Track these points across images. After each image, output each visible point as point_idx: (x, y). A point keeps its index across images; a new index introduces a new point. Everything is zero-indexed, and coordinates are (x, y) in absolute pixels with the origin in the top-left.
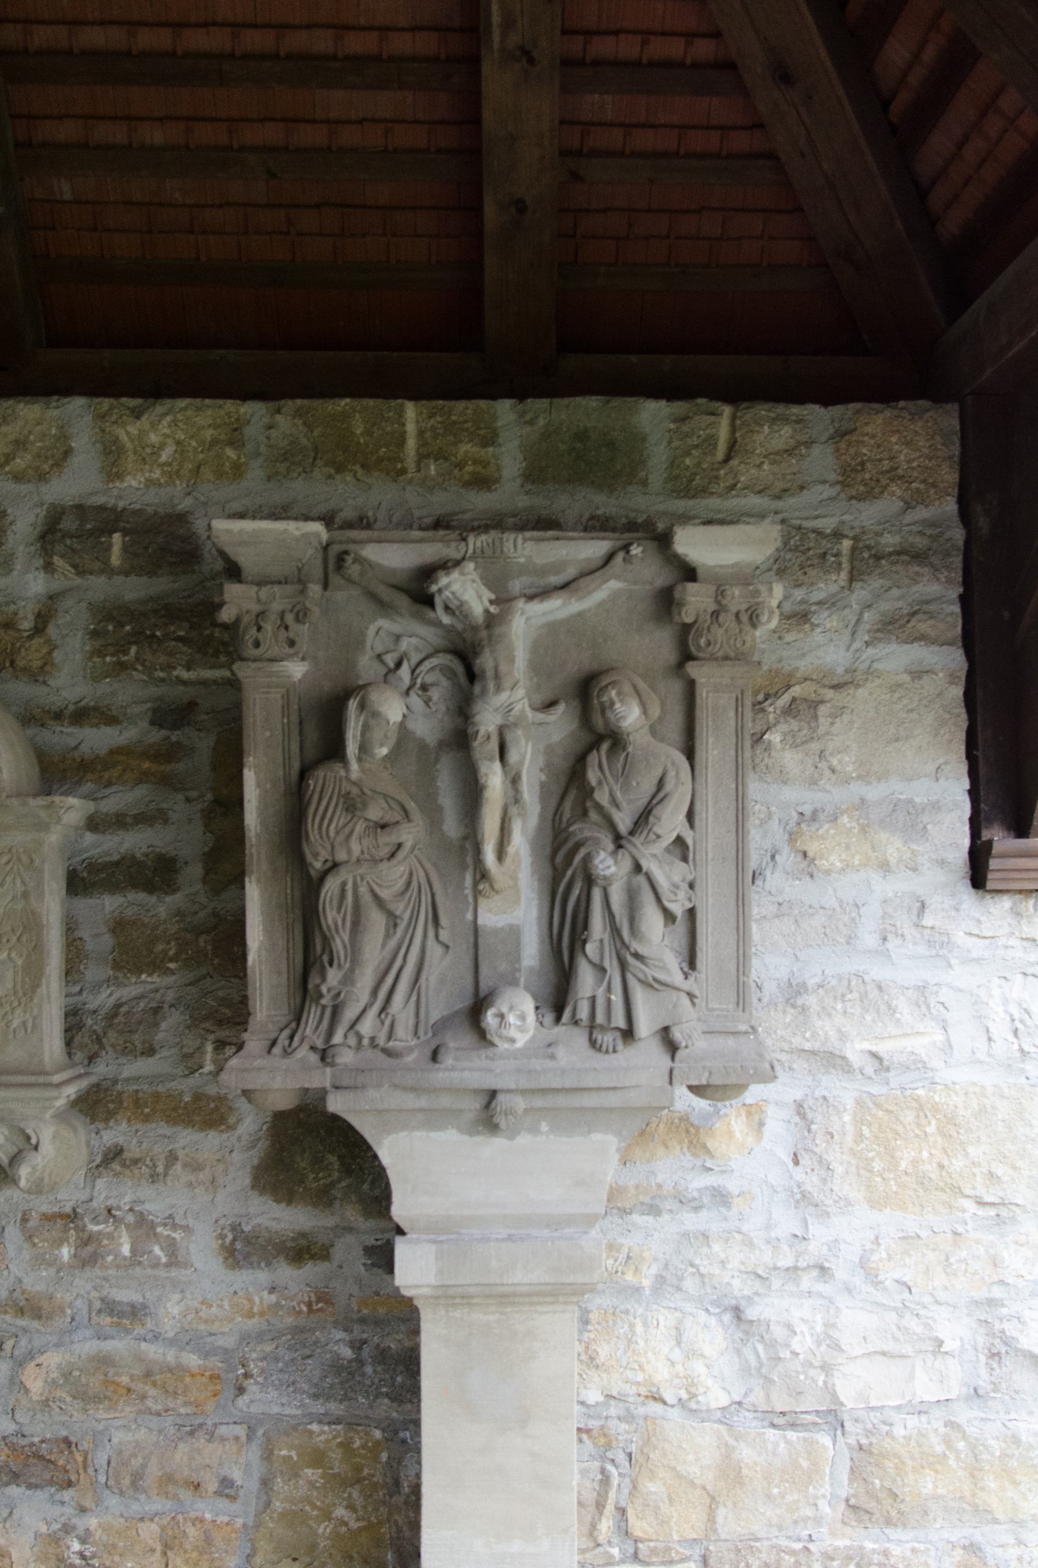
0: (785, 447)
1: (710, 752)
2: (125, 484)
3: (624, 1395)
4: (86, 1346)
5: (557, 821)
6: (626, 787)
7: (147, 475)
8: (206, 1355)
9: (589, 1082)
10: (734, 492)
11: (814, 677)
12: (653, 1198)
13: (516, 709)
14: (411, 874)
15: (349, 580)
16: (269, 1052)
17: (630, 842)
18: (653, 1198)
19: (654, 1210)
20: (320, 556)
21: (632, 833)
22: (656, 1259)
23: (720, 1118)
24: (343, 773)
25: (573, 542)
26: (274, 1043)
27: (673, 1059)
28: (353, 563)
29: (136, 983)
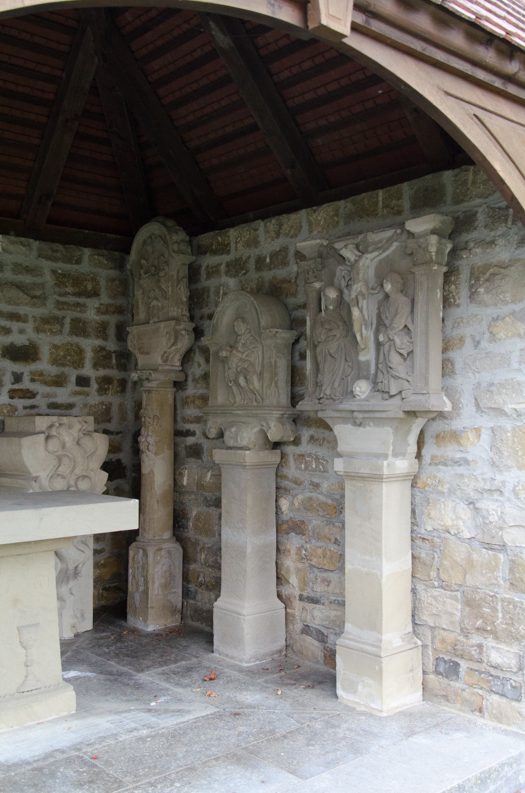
4: (308, 494)
9: (375, 409)
12: (445, 460)
14: (339, 344)
19: (445, 465)
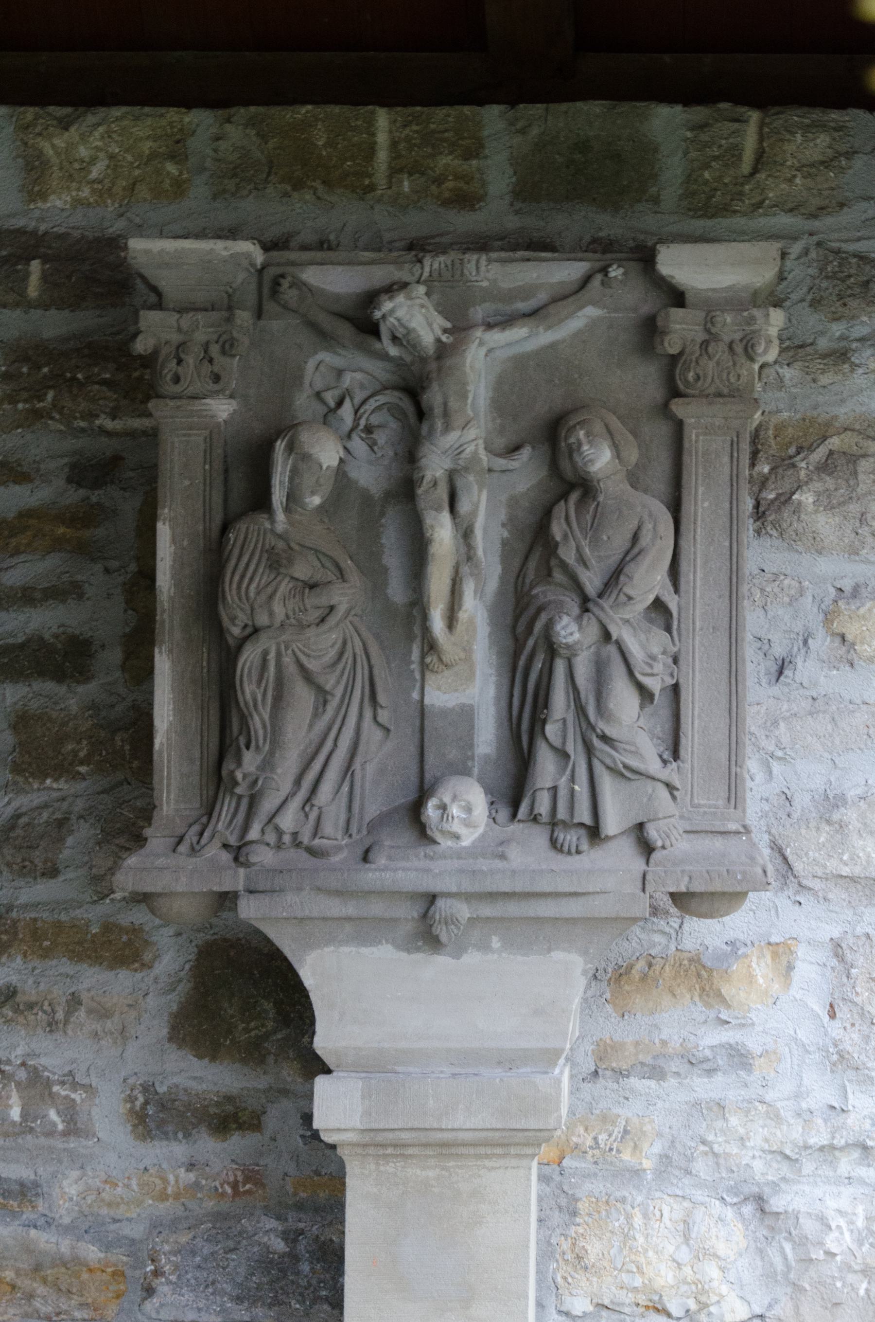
0: (821, 158)
1: (699, 503)
2: (49, 205)
3: (619, 1304)
5: (520, 583)
6: (595, 542)
7: (74, 193)
8: (107, 1247)
10: (761, 211)
11: (857, 427)
12: (655, 1058)
13: (468, 451)
14: (345, 643)
15: (285, 307)
16: (174, 851)
17: (597, 604)
18: (655, 1058)
19: (656, 1073)
20: (254, 280)
21: (600, 595)
22: (660, 1135)
23: (738, 958)
24: (268, 525)
25: (544, 264)
26: (180, 840)
27: (647, 863)
28: (290, 287)
29: (39, 789)
